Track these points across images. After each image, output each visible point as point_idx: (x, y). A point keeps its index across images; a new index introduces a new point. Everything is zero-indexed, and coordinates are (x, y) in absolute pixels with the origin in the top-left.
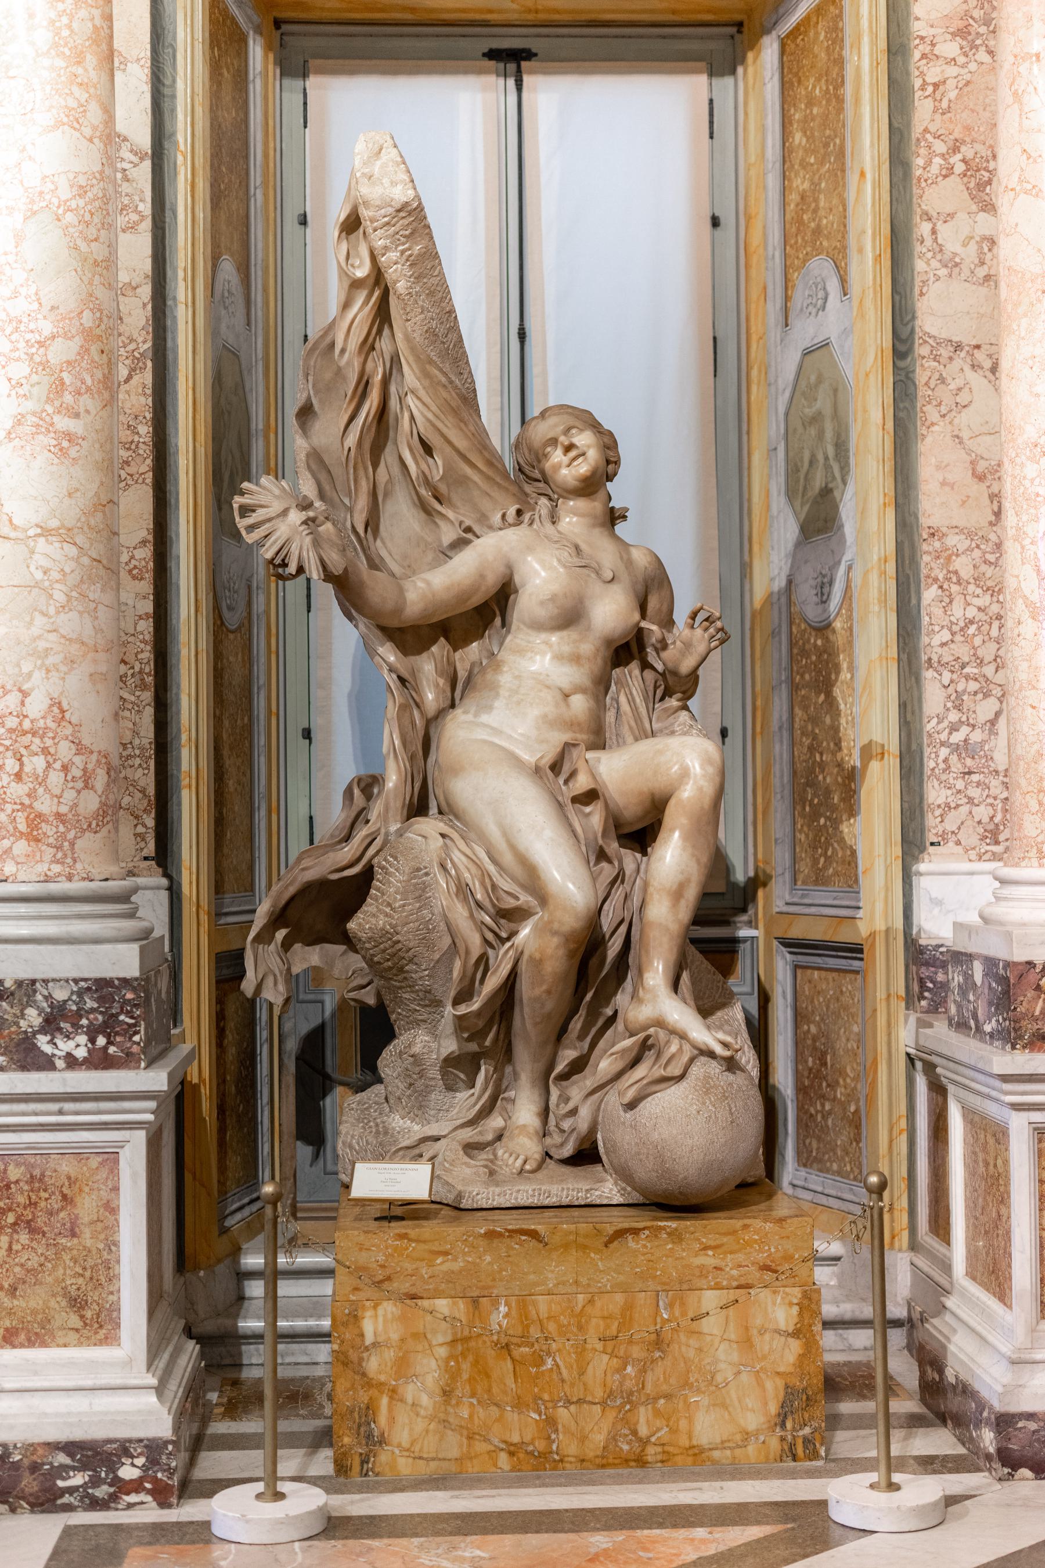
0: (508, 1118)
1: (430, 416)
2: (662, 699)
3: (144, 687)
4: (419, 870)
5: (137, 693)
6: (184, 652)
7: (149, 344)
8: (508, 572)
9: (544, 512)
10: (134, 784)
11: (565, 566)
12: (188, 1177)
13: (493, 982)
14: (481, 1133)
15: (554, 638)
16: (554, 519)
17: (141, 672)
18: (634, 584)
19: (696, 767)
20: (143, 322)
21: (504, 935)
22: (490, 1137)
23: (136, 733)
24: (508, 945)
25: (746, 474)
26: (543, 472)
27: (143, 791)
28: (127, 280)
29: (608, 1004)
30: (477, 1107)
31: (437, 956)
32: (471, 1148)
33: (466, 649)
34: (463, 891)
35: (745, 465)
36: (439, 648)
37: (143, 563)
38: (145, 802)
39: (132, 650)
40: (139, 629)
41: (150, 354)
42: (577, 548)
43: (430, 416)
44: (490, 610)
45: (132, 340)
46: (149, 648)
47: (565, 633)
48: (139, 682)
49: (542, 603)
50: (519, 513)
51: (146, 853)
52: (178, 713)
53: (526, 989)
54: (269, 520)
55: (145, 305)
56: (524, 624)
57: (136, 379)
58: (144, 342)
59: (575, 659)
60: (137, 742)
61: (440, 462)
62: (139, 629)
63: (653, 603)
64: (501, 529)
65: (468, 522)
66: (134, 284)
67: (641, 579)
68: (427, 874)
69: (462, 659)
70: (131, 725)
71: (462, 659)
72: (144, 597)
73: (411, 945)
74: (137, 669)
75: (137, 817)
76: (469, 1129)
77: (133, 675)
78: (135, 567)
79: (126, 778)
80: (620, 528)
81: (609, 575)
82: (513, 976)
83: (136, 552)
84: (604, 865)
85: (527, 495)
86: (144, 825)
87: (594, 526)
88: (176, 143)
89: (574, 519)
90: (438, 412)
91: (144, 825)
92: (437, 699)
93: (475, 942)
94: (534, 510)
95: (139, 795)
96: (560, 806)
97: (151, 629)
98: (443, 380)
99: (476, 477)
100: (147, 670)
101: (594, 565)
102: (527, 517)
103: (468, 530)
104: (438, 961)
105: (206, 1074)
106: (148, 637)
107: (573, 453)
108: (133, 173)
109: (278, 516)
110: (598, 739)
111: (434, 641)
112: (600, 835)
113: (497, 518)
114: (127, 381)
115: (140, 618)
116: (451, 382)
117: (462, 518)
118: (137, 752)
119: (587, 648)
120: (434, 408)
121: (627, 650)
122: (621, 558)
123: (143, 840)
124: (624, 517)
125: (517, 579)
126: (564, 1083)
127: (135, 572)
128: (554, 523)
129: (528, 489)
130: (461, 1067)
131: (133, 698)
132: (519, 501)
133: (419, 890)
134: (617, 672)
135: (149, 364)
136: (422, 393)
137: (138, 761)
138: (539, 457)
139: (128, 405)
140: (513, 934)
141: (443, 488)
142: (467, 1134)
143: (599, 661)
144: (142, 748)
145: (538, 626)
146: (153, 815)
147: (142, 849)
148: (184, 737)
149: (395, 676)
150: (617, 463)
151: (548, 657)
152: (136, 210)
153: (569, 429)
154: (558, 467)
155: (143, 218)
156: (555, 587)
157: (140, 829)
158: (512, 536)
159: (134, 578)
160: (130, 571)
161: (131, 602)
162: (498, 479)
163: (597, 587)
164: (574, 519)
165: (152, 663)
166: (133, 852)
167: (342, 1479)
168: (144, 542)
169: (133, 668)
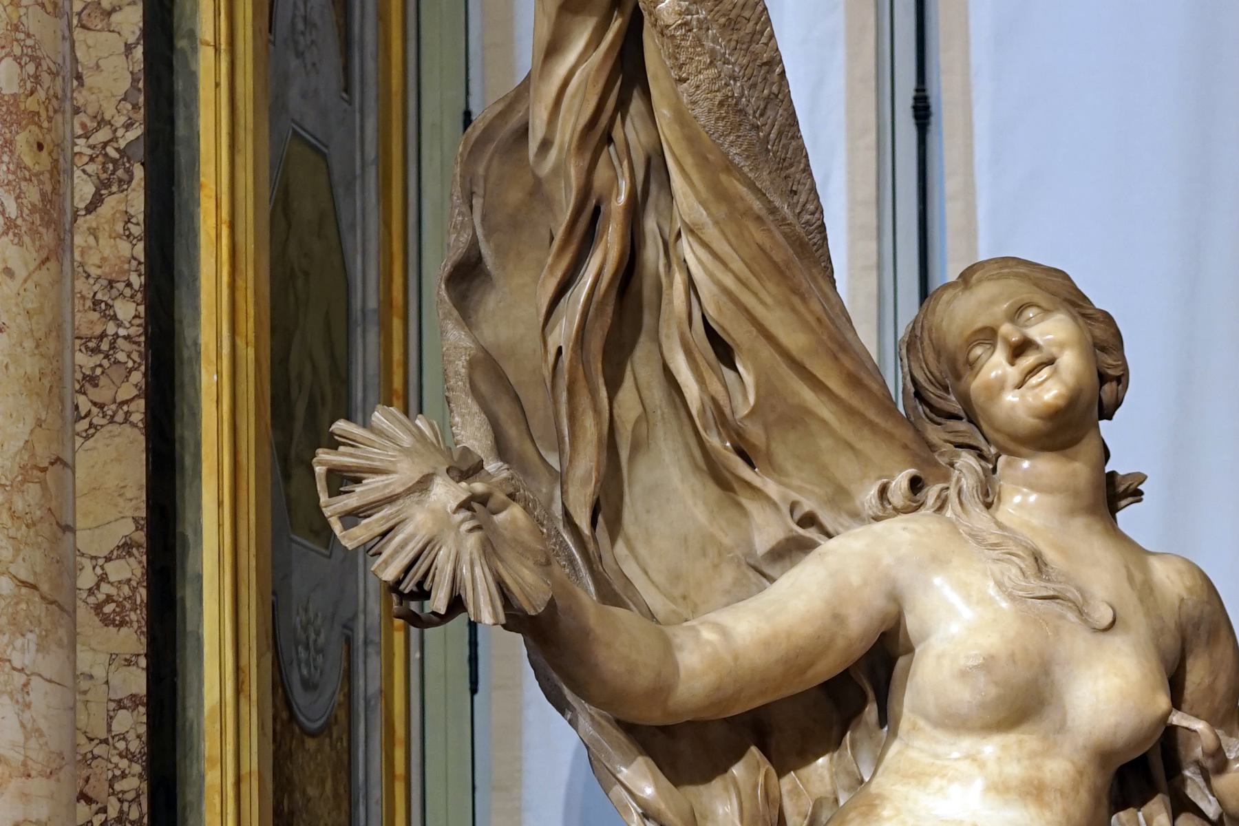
1: (729, 281)
7: (137, 132)
8: (892, 608)
11: (1012, 598)
15: (990, 747)
16: (988, 498)
18: (1157, 635)
26: (965, 400)
39: (101, 772)
41: (140, 151)
43: (729, 281)
45: (102, 122)
46: (137, 768)
50: (916, 484)
55: (129, 48)
57: (110, 204)
58: (128, 126)
62: (116, 728)
64: (877, 519)
65: (807, 505)
71: (795, 792)
78: (109, 599)
81: (1105, 616)
83: (109, 567)
85: (932, 447)
94: (946, 478)
97: (143, 729)
99: (825, 410)
101: (1073, 593)
102: (931, 493)
103: (809, 520)
107: (1029, 360)
114: (91, 208)
115: (120, 705)
116: (773, 211)
117: (795, 496)
119: (1058, 769)
120: (737, 265)
122: (1130, 579)
125: (911, 624)
127: (108, 609)
128: (988, 506)
129: (934, 434)
132: (915, 460)
135: (139, 172)
141: (755, 433)
143: (1084, 796)
145: (955, 722)
150: (1122, 380)
153: (1020, 309)
154: (999, 386)
156: (991, 641)
159: (107, 621)
160: (98, 608)
162: (872, 414)
163: (1076, 641)
168: (126, 547)
169: (104, 810)
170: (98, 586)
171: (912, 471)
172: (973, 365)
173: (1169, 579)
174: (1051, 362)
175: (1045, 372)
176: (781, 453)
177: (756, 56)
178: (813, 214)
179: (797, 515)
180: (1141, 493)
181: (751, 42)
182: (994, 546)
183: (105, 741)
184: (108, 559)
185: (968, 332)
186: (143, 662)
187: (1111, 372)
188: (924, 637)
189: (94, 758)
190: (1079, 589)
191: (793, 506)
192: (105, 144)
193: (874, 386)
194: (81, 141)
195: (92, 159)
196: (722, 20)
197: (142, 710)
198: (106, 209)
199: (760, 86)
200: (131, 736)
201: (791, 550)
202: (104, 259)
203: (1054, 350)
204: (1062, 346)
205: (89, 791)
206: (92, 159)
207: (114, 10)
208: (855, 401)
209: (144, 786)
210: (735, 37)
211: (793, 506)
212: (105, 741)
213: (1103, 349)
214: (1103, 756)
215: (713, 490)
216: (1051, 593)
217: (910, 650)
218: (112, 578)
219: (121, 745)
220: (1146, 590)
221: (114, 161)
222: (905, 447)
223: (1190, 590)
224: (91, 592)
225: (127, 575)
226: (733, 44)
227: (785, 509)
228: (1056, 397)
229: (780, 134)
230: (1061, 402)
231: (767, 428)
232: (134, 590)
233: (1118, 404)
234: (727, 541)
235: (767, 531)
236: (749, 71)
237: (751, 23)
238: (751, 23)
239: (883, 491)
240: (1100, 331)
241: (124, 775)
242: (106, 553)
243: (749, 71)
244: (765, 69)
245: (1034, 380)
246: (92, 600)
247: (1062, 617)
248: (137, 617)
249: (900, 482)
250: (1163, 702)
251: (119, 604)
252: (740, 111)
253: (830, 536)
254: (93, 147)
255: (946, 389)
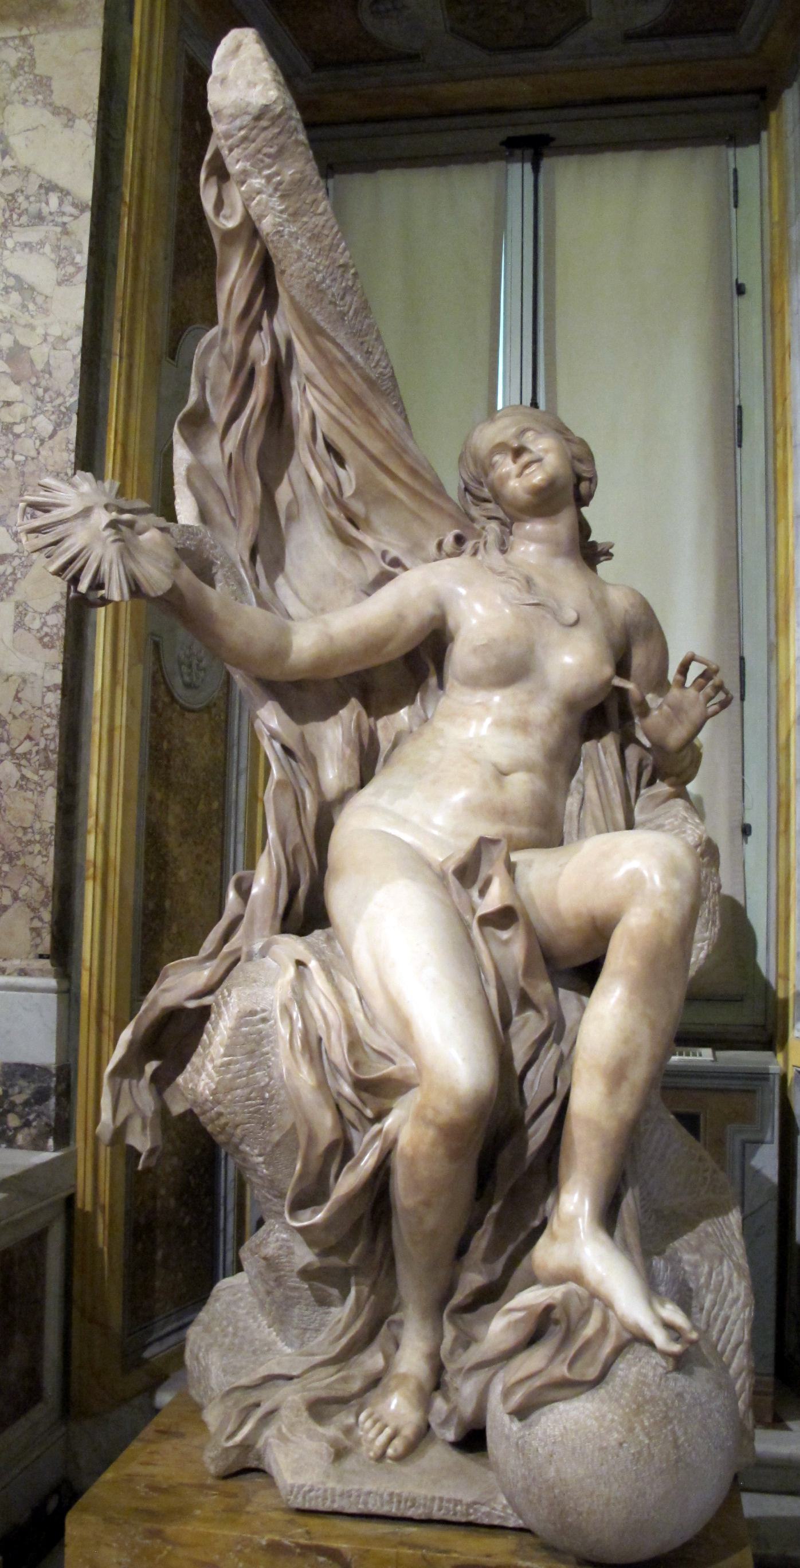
0: (388, 1359)
1: (334, 411)
2: (651, 783)
3: (47, 765)
4: (254, 1013)
5: (41, 772)
6: (96, 728)
7: (76, 398)
8: (438, 612)
9: (491, 538)
10: (32, 872)
11: (511, 604)
12: (76, 1314)
13: (347, 1182)
14: (345, 1380)
15: (496, 698)
16: (503, 547)
17: (45, 749)
18: (608, 629)
19: (656, 879)
20: (71, 374)
21: (369, 1113)
22: (356, 1386)
23: (37, 816)
24: (376, 1127)
25: (778, 368)
26: (492, 489)
27: (41, 881)
28: (59, 334)
29: (535, 1214)
30: (344, 1341)
31: (276, 1137)
32: (319, 1409)
33: (392, 717)
34: (313, 1048)
35: (772, 536)
36: (351, 712)
37: (55, 630)
38: (43, 893)
39: (37, 725)
40: (46, 701)
41: (76, 408)
42: (529, 583)
43: (334, 411)
44: (413, 665)
45: (59, 394)
46: (55, 722)
47: (509, 692)
48: (43, 760)
49: (475, 650)
50: (459, 540)
51: (41, 950)
52: (87, 794)
53: (404, 1193)
54: (61, 522)
55: (74, 357)
56: (457, 679)
57: (61, 434)
58: (71, 396)
59: (523, 726)
60: (37, 826)
61: (352, 474)
62: (46, 701)
63: (638, 658)
64: (435, 560)
65: (393, 553)
66: (65, 337)
67: (618, 624)
68: (264, 1020)
69: (385, 727)
70: (32, 807)
71: (385, 727)
72: (54, 667)
73: (238, 1119)
74: (42, 746)
75: (34, 910)
76: (332, 1369)
77: (37, 752)
78: (47, 634)
79: (24, 866)
80: (603, 567)
81: (571, 616)
82: (383, 1171)
83: (48, 618)
84: (530, 1014)
85: (473, 520)
86: (41, 919)
87: (556, 554)
88: (122, 195)
89: (533, 546)
90: (342, 404)
91: (41, 919)
92: (340, 777)
93: (325, 1124)
94: (479, 536)
95: (36, 885)
96: (466, 928)
97: (59, 702)
98: (340, 356)
99: (401, 494)
100: (52, 747)
101: (551, 603)
102: (469, 545)
103: (396, 563)
104: (278, 1144)
105: (105, 1198)
106: (55, 711)
107: (525, 458)
108: (73, 226)
109: (76, 517)
110: (549, 831)
111: (343, 702)
112: (520, 972)
113: (432, 548)
114: (51, 437)
115: (49, 689)
116: (350, 359)
117: (385, 547)
118: (38, 837)
119: (542, 710)
120: (336, 398)
121: (601, 714)
122: (591, 596)
123: (39, 935)
124: (608, 555)
125: (451, 623)
126: (468, 1317)
127: (46, 639)
128: (503, 552)
129: (475, 512)
130: (324, 1281)
131: (36, 778)
132: (458, 524)
133: (252, 1041)
134: (588, 746)
135: (75, 418)
136: (320, 380)
137: (37, 848)
138: (484, 467)
139: (51, 461)
140: (380, 1116)
141: (358, 507)
142: (323, 1382)
143: (556, 728)
144: (42, 834)
145: (475, 681)
146: (50, 908)
147: (37, 946)
148: (91, 822)
149: (277, 745)
150: (592, 480)
151: (489, 720)
152: (73, 263)
153: (524, 431)
154: (507, 477)
155: (79, 269)
156: (496, 631)
157: (37, 924)
158: (448, 566)
159: (45, 646)
160: (41, 639)
161: (39, 673)
162: (428, 494)
163: (555, 634)
164: (533, 546)
165: (57, 740)
166: (28, 949)
167: (372, 1462)
168: (56, 608)
169: (37, 744)
170: (42, 628)
171: (457, 531)
172: (493, 466)
173: (619, 600)
174: (539, 460)
175: (534, 467)
176: (376, 520)
177: (334, 261)
178: (385, 368)
179: (388, 559)
180: (612, 555)
181: (330, 250)
182: (501, 574)
183: (40, 708)
184: (47, 614)
185: (491, 446)
186: (61, 667)
187: (585, 475)
188: (458, 628)
189: (35, 717)
190: (556, 600)
191: (384, 554)
192: (60, 405)
193: (428, 477)
194: (49, 405)
195: (53, 413)
196: (309, 235)
197: (59, 692)
198: (57, 438)
199: (339, 280)
200: (53, 706)
201: (383, 579)
202: (55, 462)
203: (541, 454)
204: (546, 451)
205: (32, 735)
206: (53, 413)
207: (68, 339)
208: (417, 486)
209: (58, 732)
210: (318, 246)
211: (384, 554)
212: (40, 708)
213: (580, 461)
214: (571, 705)
215: (339, 546)
216: (535, 602)
217: (452, 639)
218: (50, 623)
219: (48, 710)
220: (602, 604)
221: (64, 414)
222: (451, 516)
223: (632, 605)
224: (38, 631)
225: (55, 622)
226: (317, 251)
227: (379, 555)
228: (542, 480)
229: (356, 313)
230: (543, 484)
231: (366, 504)
232: (59, 630)
233: (591, 496)
234: (348, 575)
235: (373, 569)
236: (330, 269)
237: (330, 238)
238: (330, 238)
239: (440, 545)
240: (576, 449)
241: (48, 726)
242: (45, 611)
243: (330, 269)
244: (342, 269)
245: (527, 471)
246: (38, 635)
247: (543, 617)
248: (59, 644)
249: (449, 540)
250: (608, 670)
251: (52, 637)
252: (321, 291)
253: (406, 569)
254: (54, 407)
255: (481, 484)
